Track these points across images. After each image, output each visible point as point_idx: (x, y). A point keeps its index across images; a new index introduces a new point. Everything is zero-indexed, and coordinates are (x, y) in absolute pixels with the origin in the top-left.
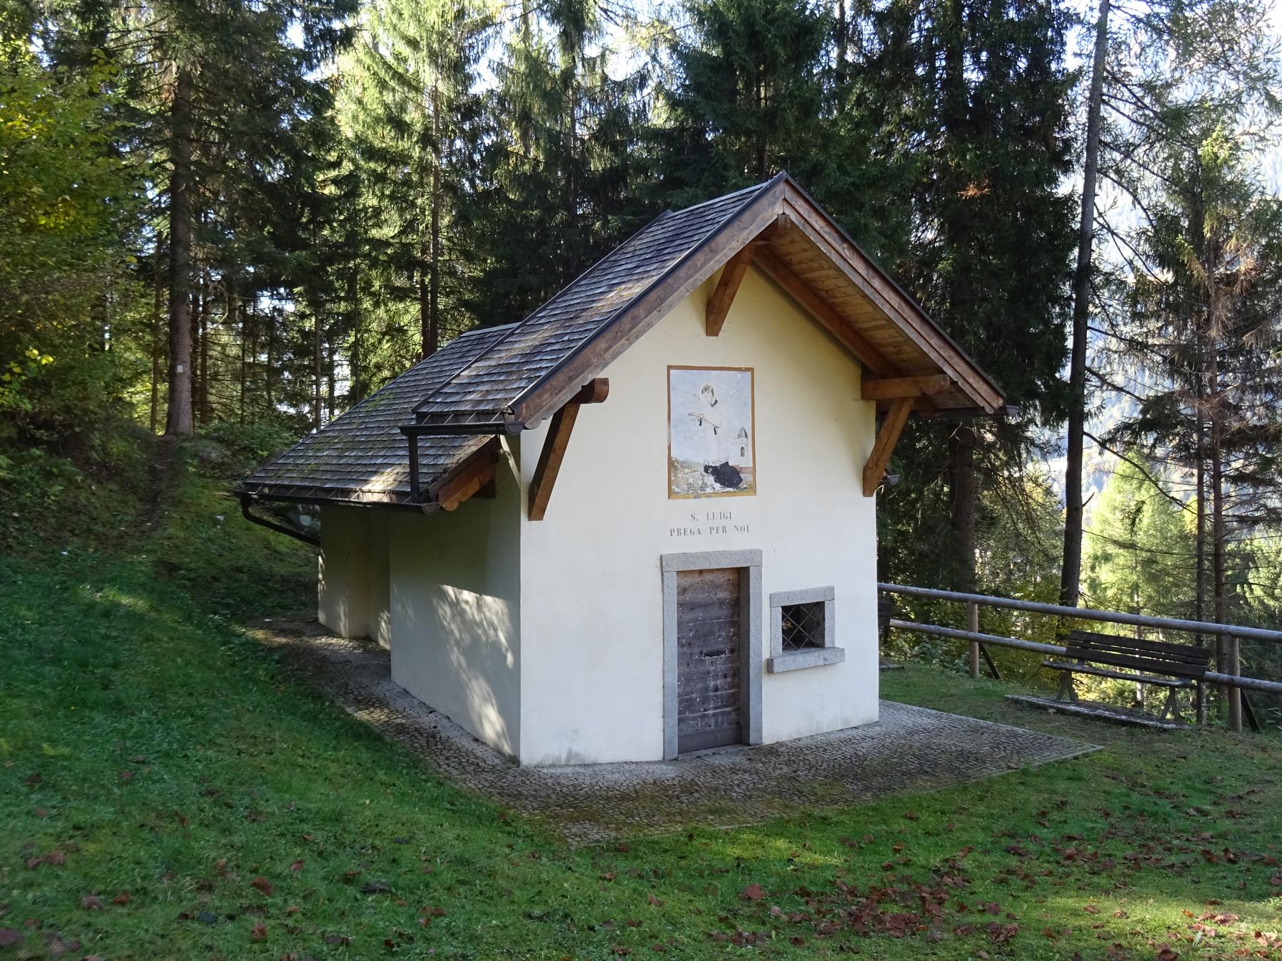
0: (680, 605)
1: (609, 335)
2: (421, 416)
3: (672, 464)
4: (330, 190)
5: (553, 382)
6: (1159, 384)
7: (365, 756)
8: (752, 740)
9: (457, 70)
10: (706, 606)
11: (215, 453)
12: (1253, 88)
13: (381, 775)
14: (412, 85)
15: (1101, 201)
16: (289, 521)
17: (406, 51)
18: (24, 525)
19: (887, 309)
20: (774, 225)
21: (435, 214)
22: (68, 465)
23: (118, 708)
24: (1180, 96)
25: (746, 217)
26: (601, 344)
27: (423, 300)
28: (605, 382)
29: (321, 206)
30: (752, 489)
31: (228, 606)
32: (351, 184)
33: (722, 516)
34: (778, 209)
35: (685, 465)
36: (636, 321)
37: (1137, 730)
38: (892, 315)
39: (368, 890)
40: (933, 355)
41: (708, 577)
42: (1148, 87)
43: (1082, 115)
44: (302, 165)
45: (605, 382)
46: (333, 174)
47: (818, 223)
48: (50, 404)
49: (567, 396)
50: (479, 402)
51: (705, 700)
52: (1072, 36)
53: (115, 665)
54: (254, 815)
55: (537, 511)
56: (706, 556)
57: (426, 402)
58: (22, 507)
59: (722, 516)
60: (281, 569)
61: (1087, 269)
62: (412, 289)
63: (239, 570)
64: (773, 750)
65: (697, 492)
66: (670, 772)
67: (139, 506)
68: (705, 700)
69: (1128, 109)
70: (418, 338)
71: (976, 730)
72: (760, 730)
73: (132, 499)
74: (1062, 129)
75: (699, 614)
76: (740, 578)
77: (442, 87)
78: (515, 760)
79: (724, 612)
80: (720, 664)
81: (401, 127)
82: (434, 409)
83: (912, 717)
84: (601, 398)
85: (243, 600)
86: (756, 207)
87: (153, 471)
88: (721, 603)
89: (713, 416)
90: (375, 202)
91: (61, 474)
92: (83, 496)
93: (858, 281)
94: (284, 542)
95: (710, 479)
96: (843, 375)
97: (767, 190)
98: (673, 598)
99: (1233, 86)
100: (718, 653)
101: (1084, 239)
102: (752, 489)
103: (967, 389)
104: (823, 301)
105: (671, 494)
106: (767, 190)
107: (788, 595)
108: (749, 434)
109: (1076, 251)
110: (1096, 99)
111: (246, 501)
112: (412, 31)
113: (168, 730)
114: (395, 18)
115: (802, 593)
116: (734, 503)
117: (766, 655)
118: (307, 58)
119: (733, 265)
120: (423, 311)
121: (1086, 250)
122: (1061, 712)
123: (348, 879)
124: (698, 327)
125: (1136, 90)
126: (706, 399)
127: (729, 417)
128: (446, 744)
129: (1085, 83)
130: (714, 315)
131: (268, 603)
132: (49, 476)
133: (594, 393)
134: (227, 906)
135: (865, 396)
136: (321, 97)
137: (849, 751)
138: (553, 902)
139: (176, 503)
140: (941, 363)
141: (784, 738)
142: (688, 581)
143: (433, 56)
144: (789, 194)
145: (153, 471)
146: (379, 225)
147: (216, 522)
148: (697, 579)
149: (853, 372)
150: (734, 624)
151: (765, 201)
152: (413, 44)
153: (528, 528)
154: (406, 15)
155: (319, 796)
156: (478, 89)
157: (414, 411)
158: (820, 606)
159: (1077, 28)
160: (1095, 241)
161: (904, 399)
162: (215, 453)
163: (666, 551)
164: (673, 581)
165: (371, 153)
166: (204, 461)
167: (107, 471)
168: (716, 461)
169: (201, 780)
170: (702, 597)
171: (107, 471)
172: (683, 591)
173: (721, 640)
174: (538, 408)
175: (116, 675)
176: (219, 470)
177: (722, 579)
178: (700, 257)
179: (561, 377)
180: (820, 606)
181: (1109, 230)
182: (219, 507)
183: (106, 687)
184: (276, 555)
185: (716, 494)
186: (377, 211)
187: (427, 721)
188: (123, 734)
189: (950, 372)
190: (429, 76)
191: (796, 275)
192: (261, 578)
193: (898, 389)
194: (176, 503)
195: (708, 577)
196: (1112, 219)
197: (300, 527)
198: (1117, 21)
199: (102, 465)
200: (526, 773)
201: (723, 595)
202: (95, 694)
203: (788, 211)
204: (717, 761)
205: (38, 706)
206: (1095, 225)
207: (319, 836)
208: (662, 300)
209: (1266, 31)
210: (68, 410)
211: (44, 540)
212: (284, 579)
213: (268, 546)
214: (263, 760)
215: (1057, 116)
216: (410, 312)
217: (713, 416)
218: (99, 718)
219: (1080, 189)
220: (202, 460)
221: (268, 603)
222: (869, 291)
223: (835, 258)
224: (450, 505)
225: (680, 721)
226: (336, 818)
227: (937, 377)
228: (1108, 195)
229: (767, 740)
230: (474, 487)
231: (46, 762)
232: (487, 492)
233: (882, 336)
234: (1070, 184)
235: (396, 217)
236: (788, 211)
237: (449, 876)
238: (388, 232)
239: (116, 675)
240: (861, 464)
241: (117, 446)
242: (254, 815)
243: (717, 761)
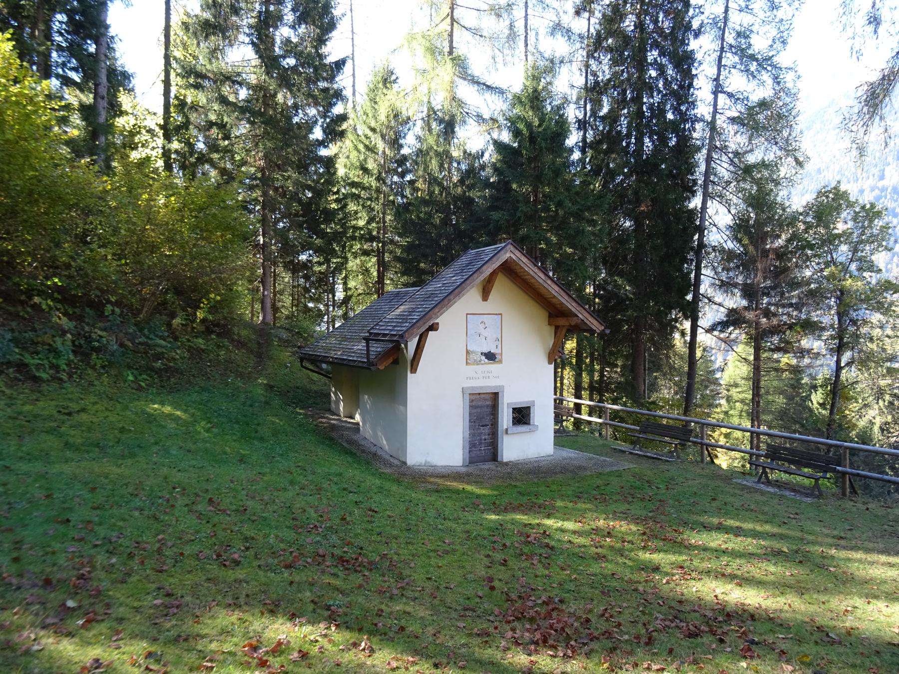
0: (470, 406)
1: (439, 306)
2: (371, 334)
3: (468, 352)
4: (334, 206)
5: (418, 325)
6: (736, 301)
7: (349, 459)
8: (499, 459)
9: (395, 143)
10: (481, 407)
11: (285, 335)
12: (788, 155)
13: (355, 465)
14: (371, 149)
15: (710, 211)
16: (317, 367)
17: (370, 133)
18: (212, 368)
19: (553, 292)
20: (506, 261)
21: (384, 213)
22: (226, 342)
23: (262, 439)
24: (752, 159)
25: (495, 259)
26: (436, 310)
27: (378, 256)
28: (438, 324)
29: (329, 215)
30: (500, 361)
31: (294, 403)
32: (342, 201)
33: (488, 372)
34: (508, 255)
35: (473, 352)
36: (450, 301)
37: (657, 462)
38: (556, 294)
39: (351, 492)
40: (573, 310)
41: (482, 396)
42: (736, 154)
43: (703, 167)
44: (320, 194)
45: (438, 324)
46: (335, 197)
47: (524, 260)
48: (220, 316)
49: (423, 329)
50: (391, 330)
51: (480, 444)
52: (699, 126)
53: (258, 425)
54: (314, 473)
55: (414, 370)
56: (481, 388)
57: (372, 328)
58: (210, 361)
59: (488, 372)
60: (315, 388)
61: (702, 245)
62: (373, 251)
63: (298, 388)
64: (507, 464)
65: (478, 363)
66: (464, 470)
67: (255, 359)
68: (480, 444)
69: (725, 165)
70: (375, 274)
71: (590, 459)
72: (502, 456)
73: (252, 356)
74: (692, 174)
75: (479, 410)
76: (495, 396)
77: (388, 152)
78: (405, 463)
79: (489, 410)
80: (487, 430)
81: (365, 170)
82: (375, 331)
83: (568, 454)
84: (437, 330)
85: (300, 400)
86: (498, 255)
87: (259, 343)
88: (488, 406)
89: (485, 333)
90: (355, 208)
91: (224, 346)
92: (233, 355)
93: (541, 281)
94: (315, 376)
95: (483, 358)
96: (541, 316)
97: (503, 248)
98: (468, 403)
99: (779, 153)
100: (486, 425)
101: (701, 230)
102: (500, 361)
103: (588, 323)
104: (531, 287)
105: (467, 363)
106: (503, 248)
107: (515, 403)
108: (500, 340)
109: (696, 237)
110: (709, 159)
111: (302, 360)
112: (373, 124)
113: (281, 448)
114: (365, 117)
115: (521, 403)
116: (493, 367)
117: (505, 427)
118: (322, 143)
119: (493, 275)
120: (378, 260)
121: (702, 236)
122: (631, 453)
123: (344, 489)
124: (479, 298)
125: (730, 155)
126: (483, 326)
127: (492, 333)
128: (380, 457)
129: (704, 151)
130: (485, 294)
131: (310, 402)
132: (219, 347)
133: (433, 327)
134: (309, 493)
135: (550, 324)
136: (329, 163)
137: (536, 465)
138: (407, 498)
139: (270, 358)
140: (577, 313)
141: (512, 459)
142: (473, 397)
143: (383, 137)
144: (512, 248)
145: (259, 343)
146: (357, 219)
147: (287, 367)
148: (478, 396)
149: (547, 314)
150: (492, 414)
151: (502, 252)
152: (373, 130)
153: (410, 376)
154: (370, 115)
155: (334, 469)
156: (405, 151)
157: (368, 332)
158: (529, 408)
159: (701, 124)
160: (706, 232)
161: (563, 326)
162: (285, 335)
163: (465, 386)
164: (467, 397)
165: (354, 185)
166: (280, 339)
167: (241, 344)
168: (486, 350)
169: (295, 463)
170: (480, 403)
171: (241, 344)
172: (471, 401)
173: (487, 420)
174: (412, 334)
175: (259, 428)
176: (285, 343)
177: (487, 397)
178: (475, 275)
179: (421, 322)
180: (529, 408)
181: (715, 225)
182: (288, 361)
183: (256, 432)
184: (312, 381)
185: (485, 363)
186: (356, 213)
187: (373, 449)
188: (266, 448)
189: (580, 316)
190: (381, 145)
191: (520, 277)
192: (307, 392)
193: (562, 322)
194: (270, 358)
195: (482, 396)
196: (717, 219)
197: (322, 369)
198: (720, 121)
199: (239, 342)
200: (409, 468)
201: (488, 403)
202: (253, 435)
203: (512, 256)
204: (483, 467)
205: (235, 438)
206: (707, 223)
207: (335, 479)
208: (460, 293)
209: (794, 125)
210: (225, 318)
211: (221, 374)
212: (316, 392)
213: (309, 377)
214: (314, 458)
215: (691, 168)
216: (372, 262)
217: (485, 333)
218: (256, 443)
219: (699, 206)
220: (279, 338)
221: (310, 402)
222: (546, 285)
223: (531, 273)
224: (381, 367)
225: (470, 452)
226: (340, 475)
227: (575, 318)
228: (713, 207)
229: (505, 460)
230: (391, 360)
231: (243, 456)
232: (396, 362)
233: (554, 300)
234: (696, 202)
235: (365, 215)
236: (512, 256)
237: (375, 491)
238: (361, 223)
239: (259, 428)
240: (548, 351)
241: (244, 333)
242: (314, 473)
243: (483, 467)
